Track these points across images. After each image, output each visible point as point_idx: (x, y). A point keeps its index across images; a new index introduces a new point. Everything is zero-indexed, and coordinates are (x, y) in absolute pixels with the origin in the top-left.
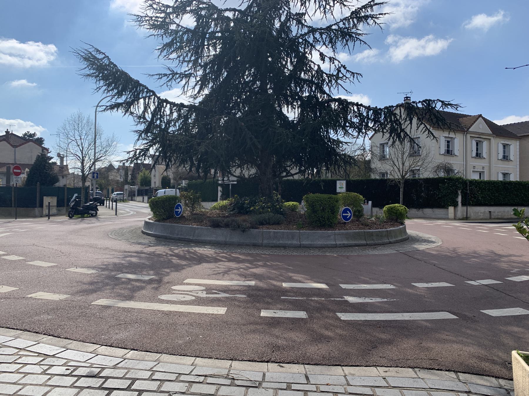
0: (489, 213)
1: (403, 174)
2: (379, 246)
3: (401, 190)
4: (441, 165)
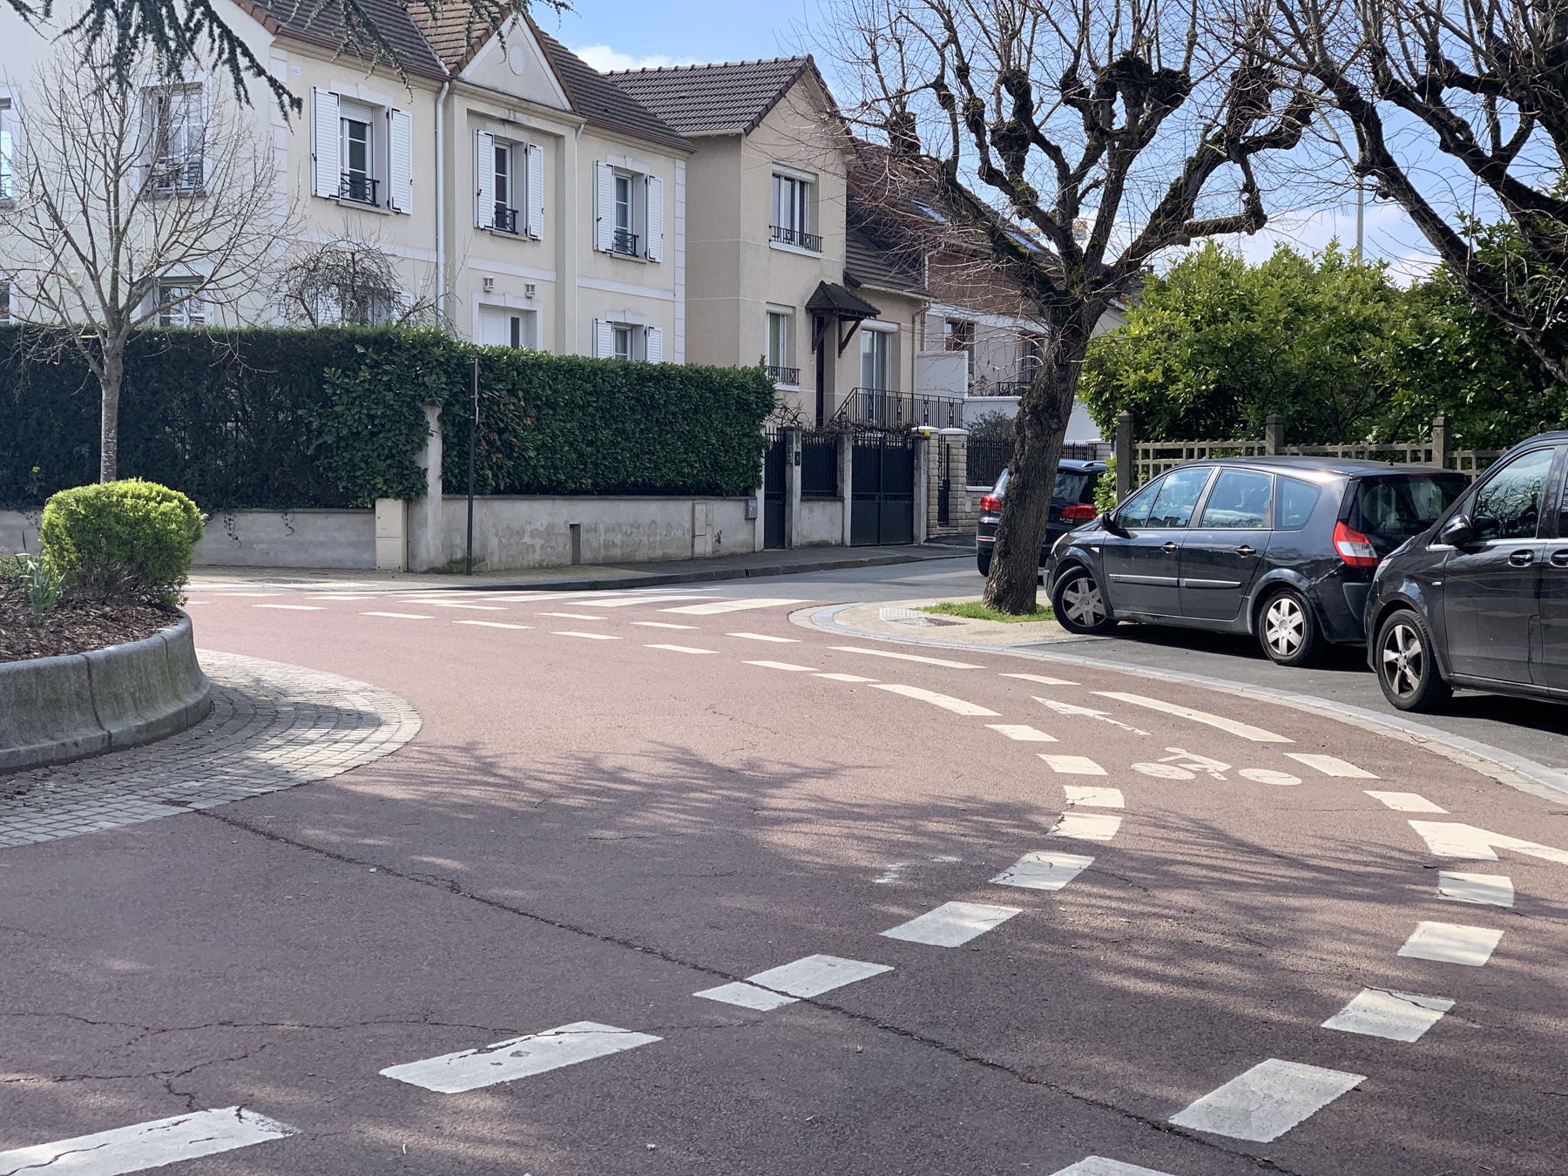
0: (568, 532)
1: (114, 298)
2: (40, 772)
3: (108, 397)
4: (326, 259)
